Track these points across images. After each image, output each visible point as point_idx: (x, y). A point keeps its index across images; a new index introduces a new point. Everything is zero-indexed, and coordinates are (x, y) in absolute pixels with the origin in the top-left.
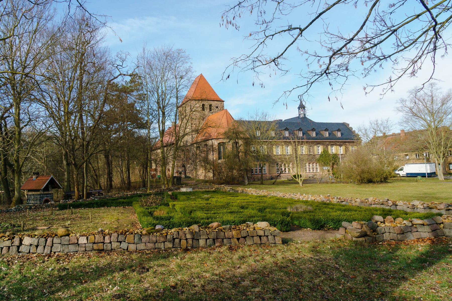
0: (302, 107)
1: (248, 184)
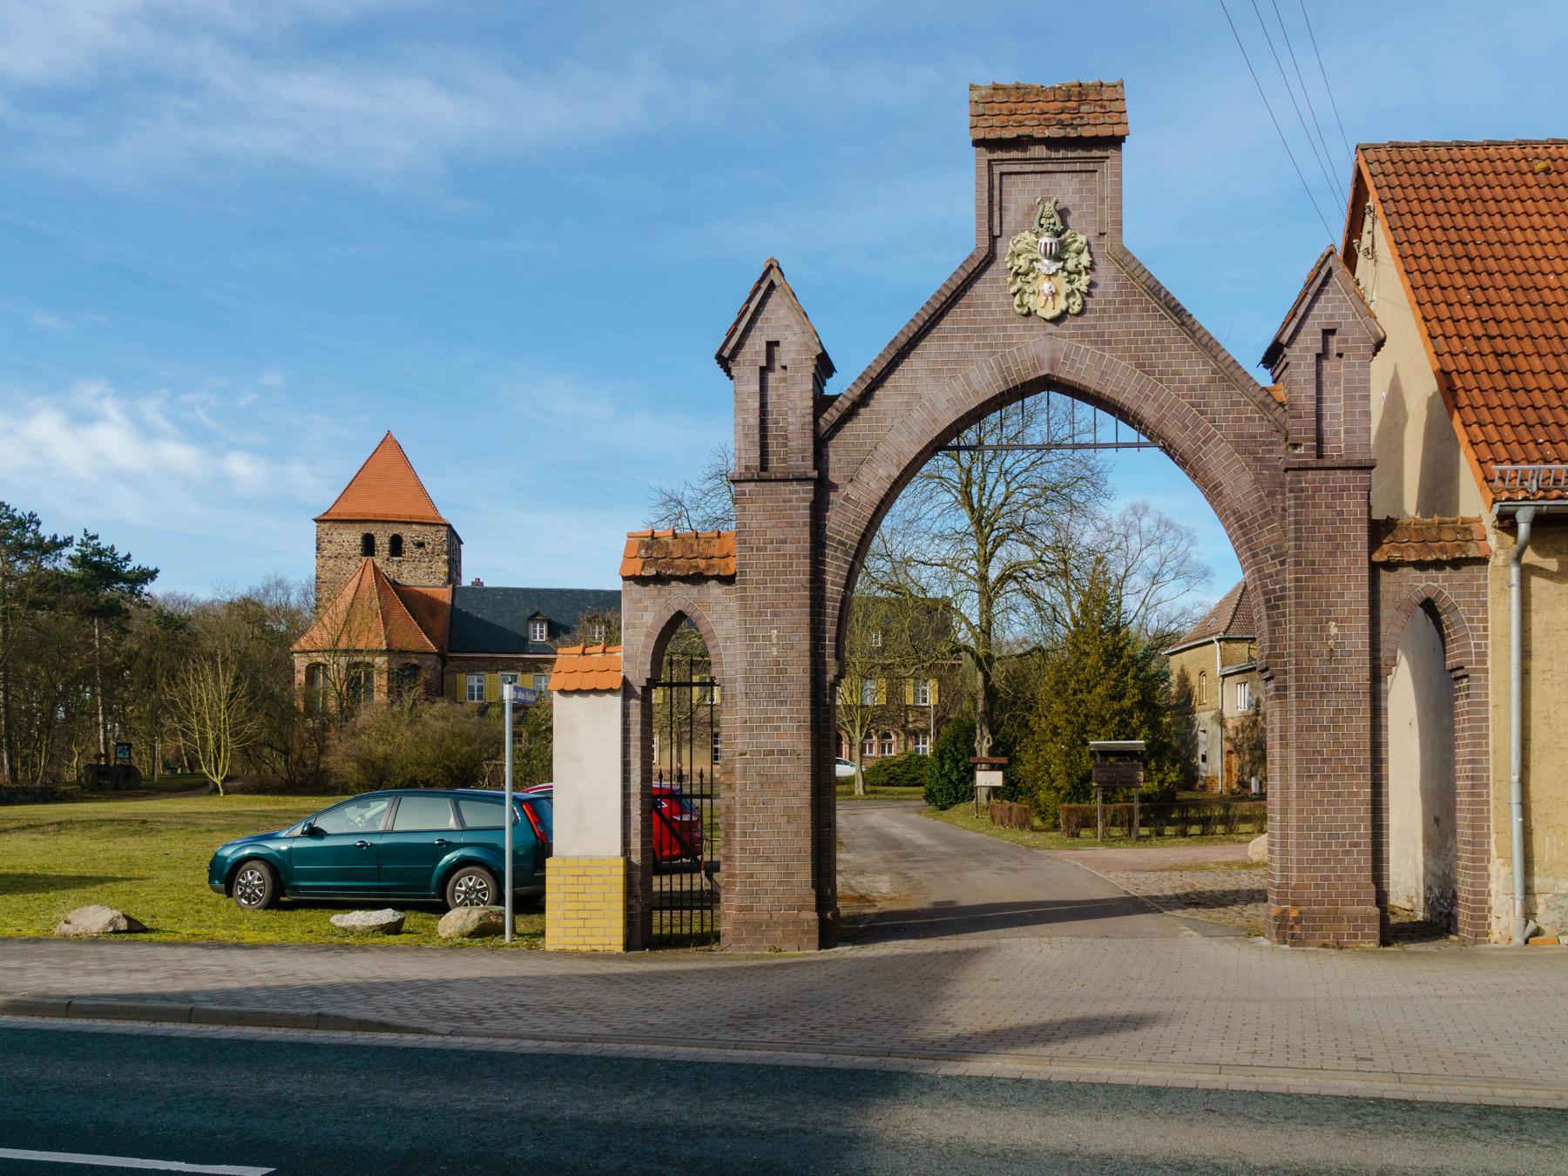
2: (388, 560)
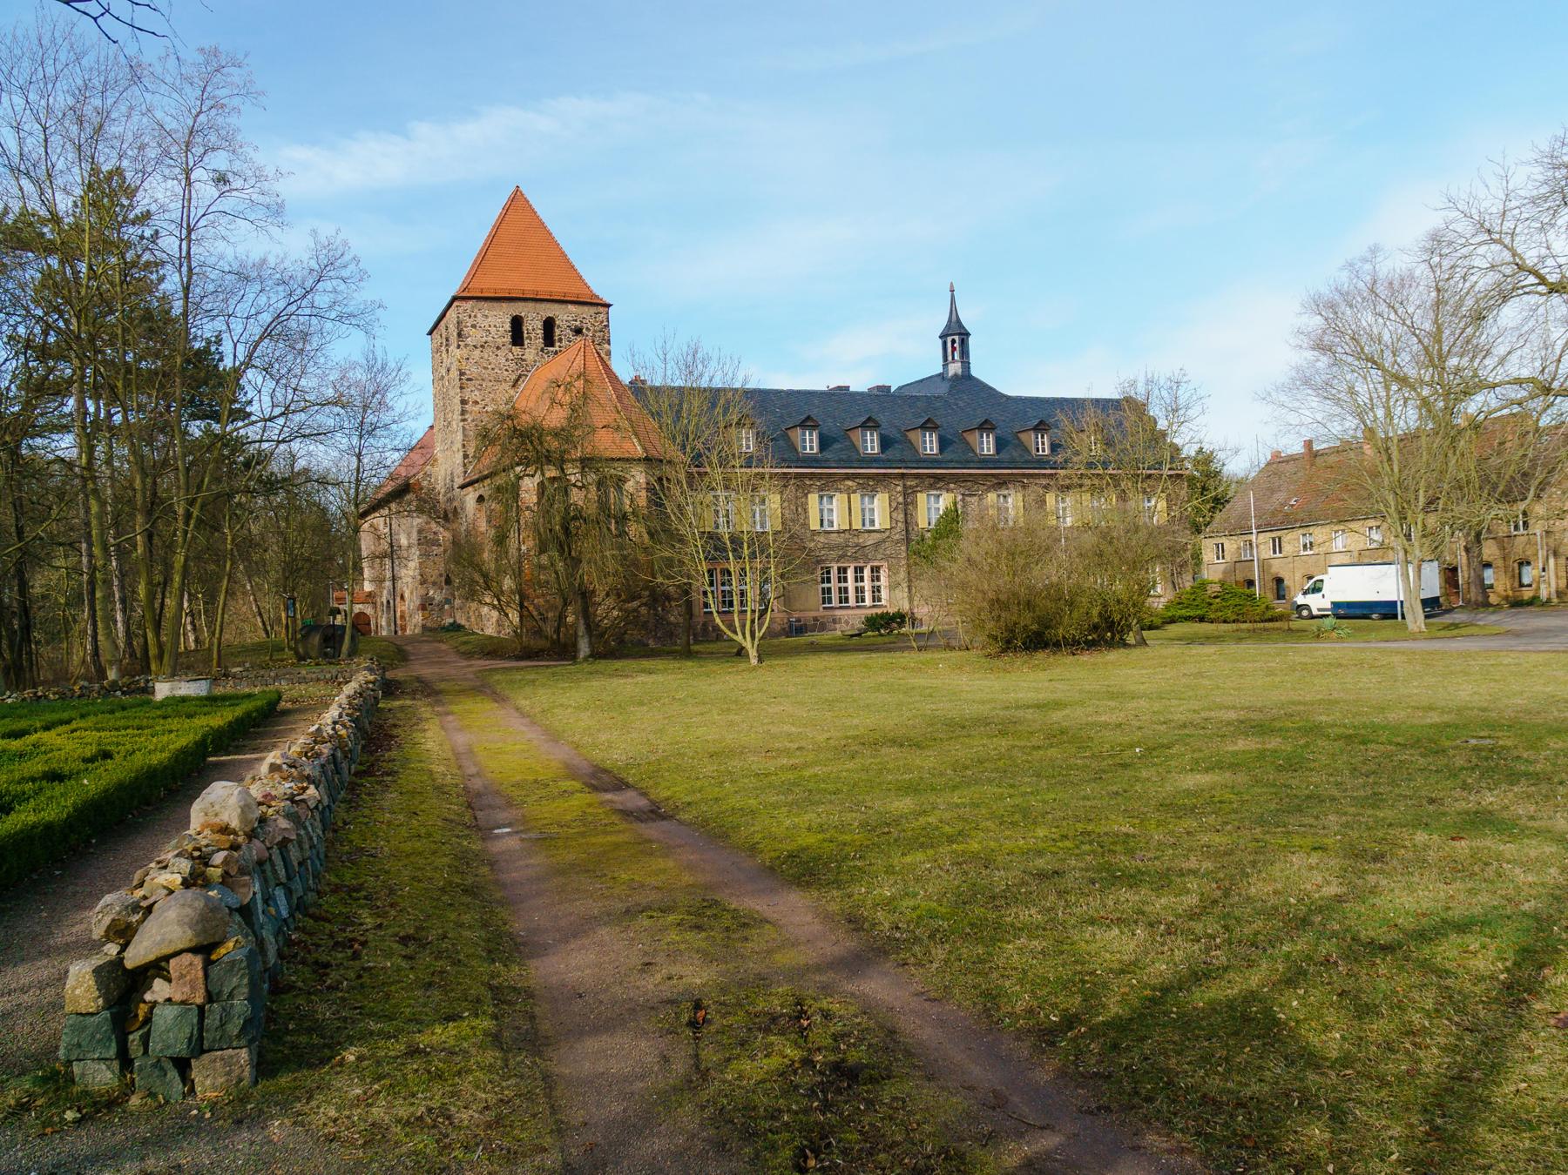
0: (956, 336)
1: (591, 656)
2: (542, 350)
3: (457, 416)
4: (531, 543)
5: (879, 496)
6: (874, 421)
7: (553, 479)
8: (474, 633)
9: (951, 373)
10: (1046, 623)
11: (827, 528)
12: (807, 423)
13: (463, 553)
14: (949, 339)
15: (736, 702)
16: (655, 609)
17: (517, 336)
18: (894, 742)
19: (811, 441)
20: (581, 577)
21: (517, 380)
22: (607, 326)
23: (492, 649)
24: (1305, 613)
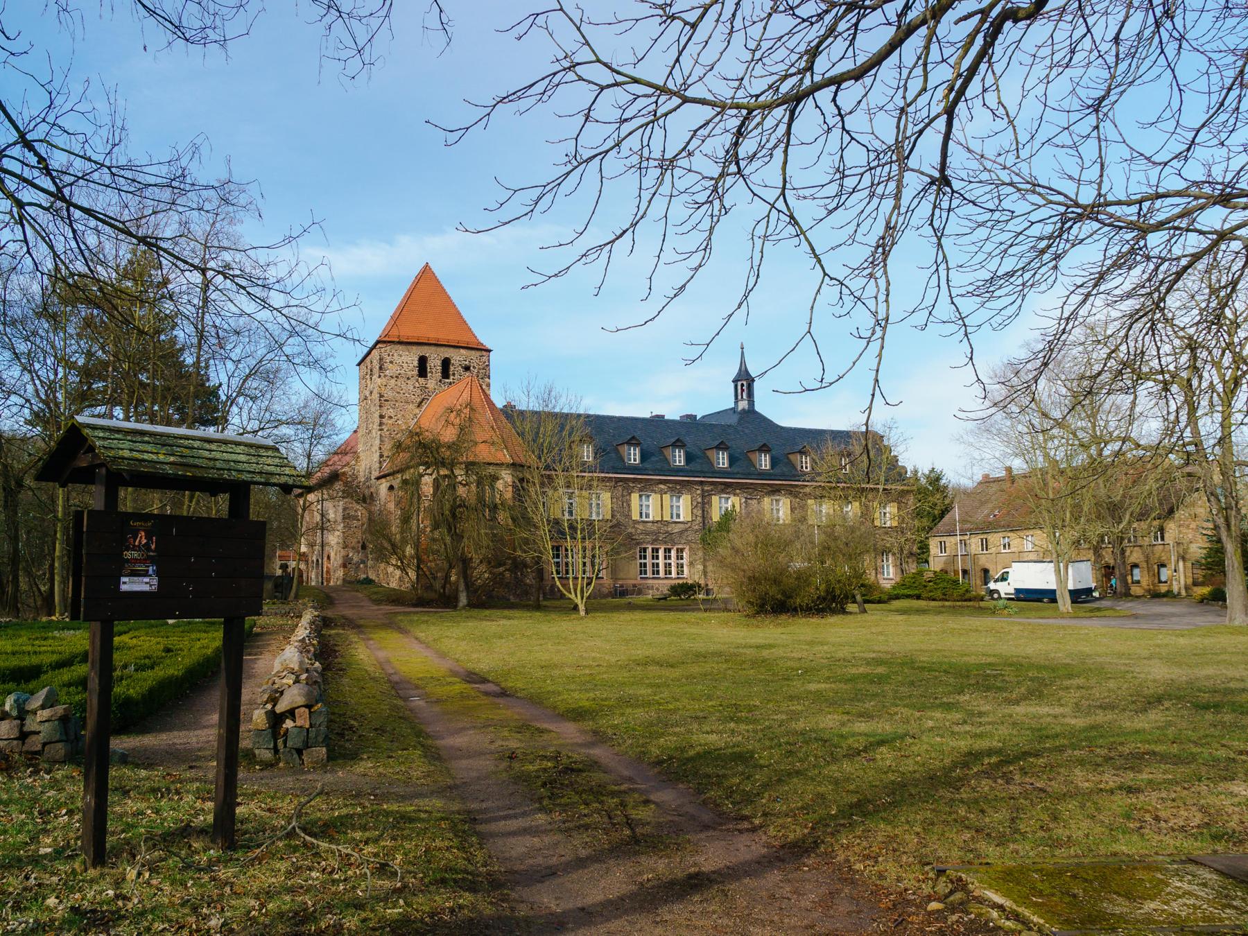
0: (744, 382)
3: (376, 427)
4: (427, 522)
5: (683, 497)
6: (681, 441)
7: (446, 476)
8: (382, 586)
9: (740, 408)
10: (788, 595)
11: (644, 519)
12: (633, 442)
13: (376, 526)
14: (739, 383)
15: (565, 639)
16: (516, 573)
17: (422, 370)
18: (658, 663)
19: (635, 454)
20: (463, 548)
21: (421, 402)
22: (488, 365)
23: (396, 598)
24: (996, 596)
